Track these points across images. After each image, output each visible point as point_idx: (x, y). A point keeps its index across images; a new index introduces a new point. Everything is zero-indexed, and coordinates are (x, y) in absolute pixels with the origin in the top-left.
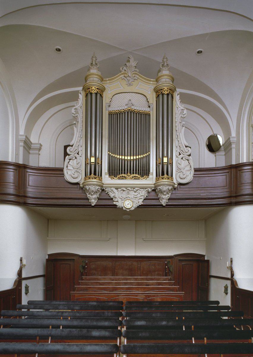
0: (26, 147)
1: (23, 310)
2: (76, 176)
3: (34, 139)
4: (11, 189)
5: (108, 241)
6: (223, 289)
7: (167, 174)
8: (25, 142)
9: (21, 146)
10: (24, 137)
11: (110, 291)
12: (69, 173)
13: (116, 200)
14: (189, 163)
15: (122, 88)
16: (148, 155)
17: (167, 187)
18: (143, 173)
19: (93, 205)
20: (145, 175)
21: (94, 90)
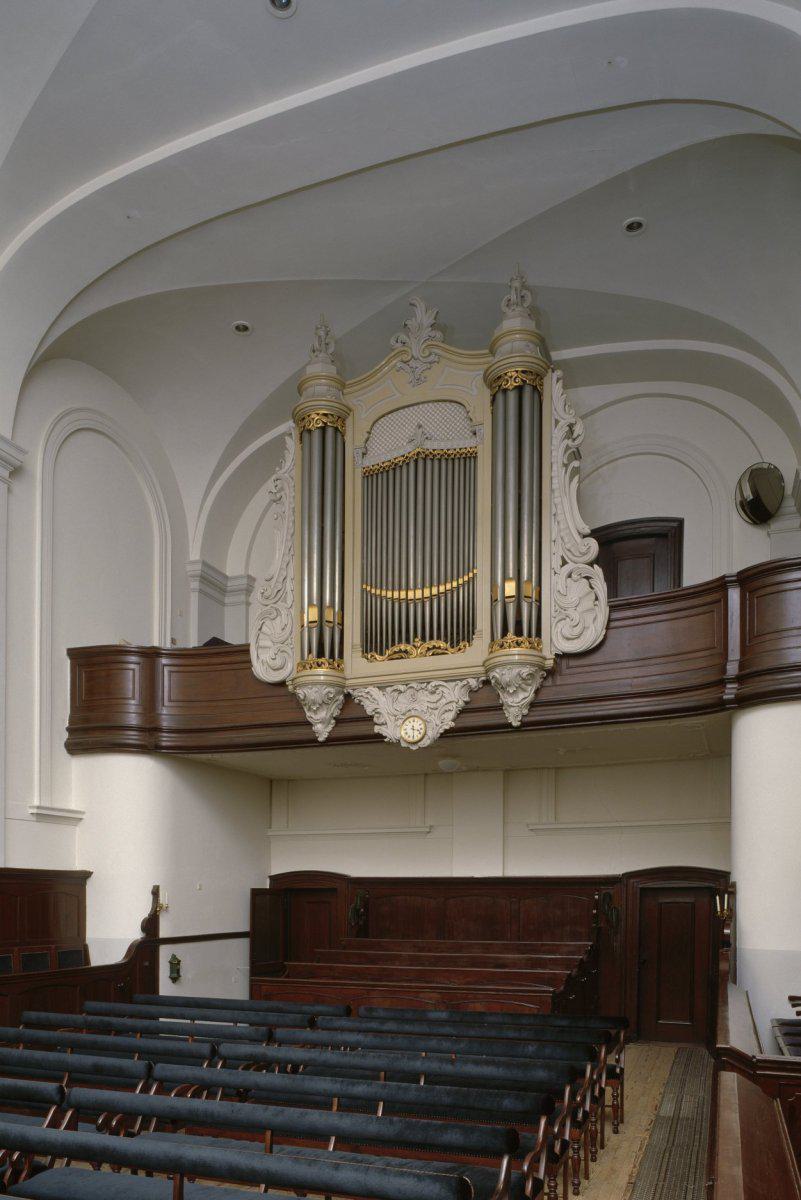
1: (161, 1020)
2: (278, 663)
3: (233, 567)
4: (792, 651)
5: (428, 836)
9: (194, 590)
11: (372, 980)
12: (262, 657)
13: (382, 720)
14: (592, 588)
15: (398, 395)
16: (469, 582)
17: (516, 671)
18: (458, 634)
19: (321, 739)
21: (316, 421)
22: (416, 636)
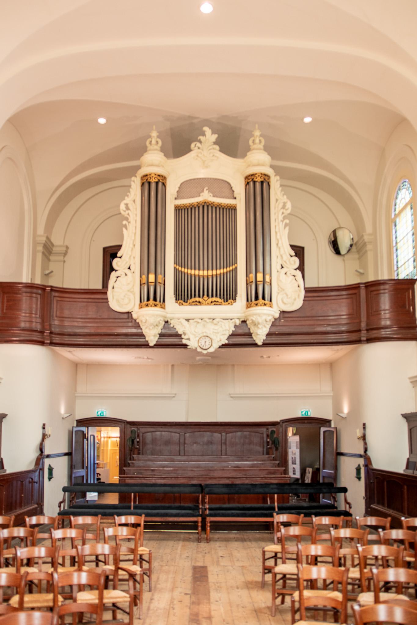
0: (45, 252)
3: (57, 240)
5: (174, 399)
6: (354, 472)
7: (264, 298)
8: (45, 246)
10: (45, 239)
20: (230, 299)
22: (203, 295)
